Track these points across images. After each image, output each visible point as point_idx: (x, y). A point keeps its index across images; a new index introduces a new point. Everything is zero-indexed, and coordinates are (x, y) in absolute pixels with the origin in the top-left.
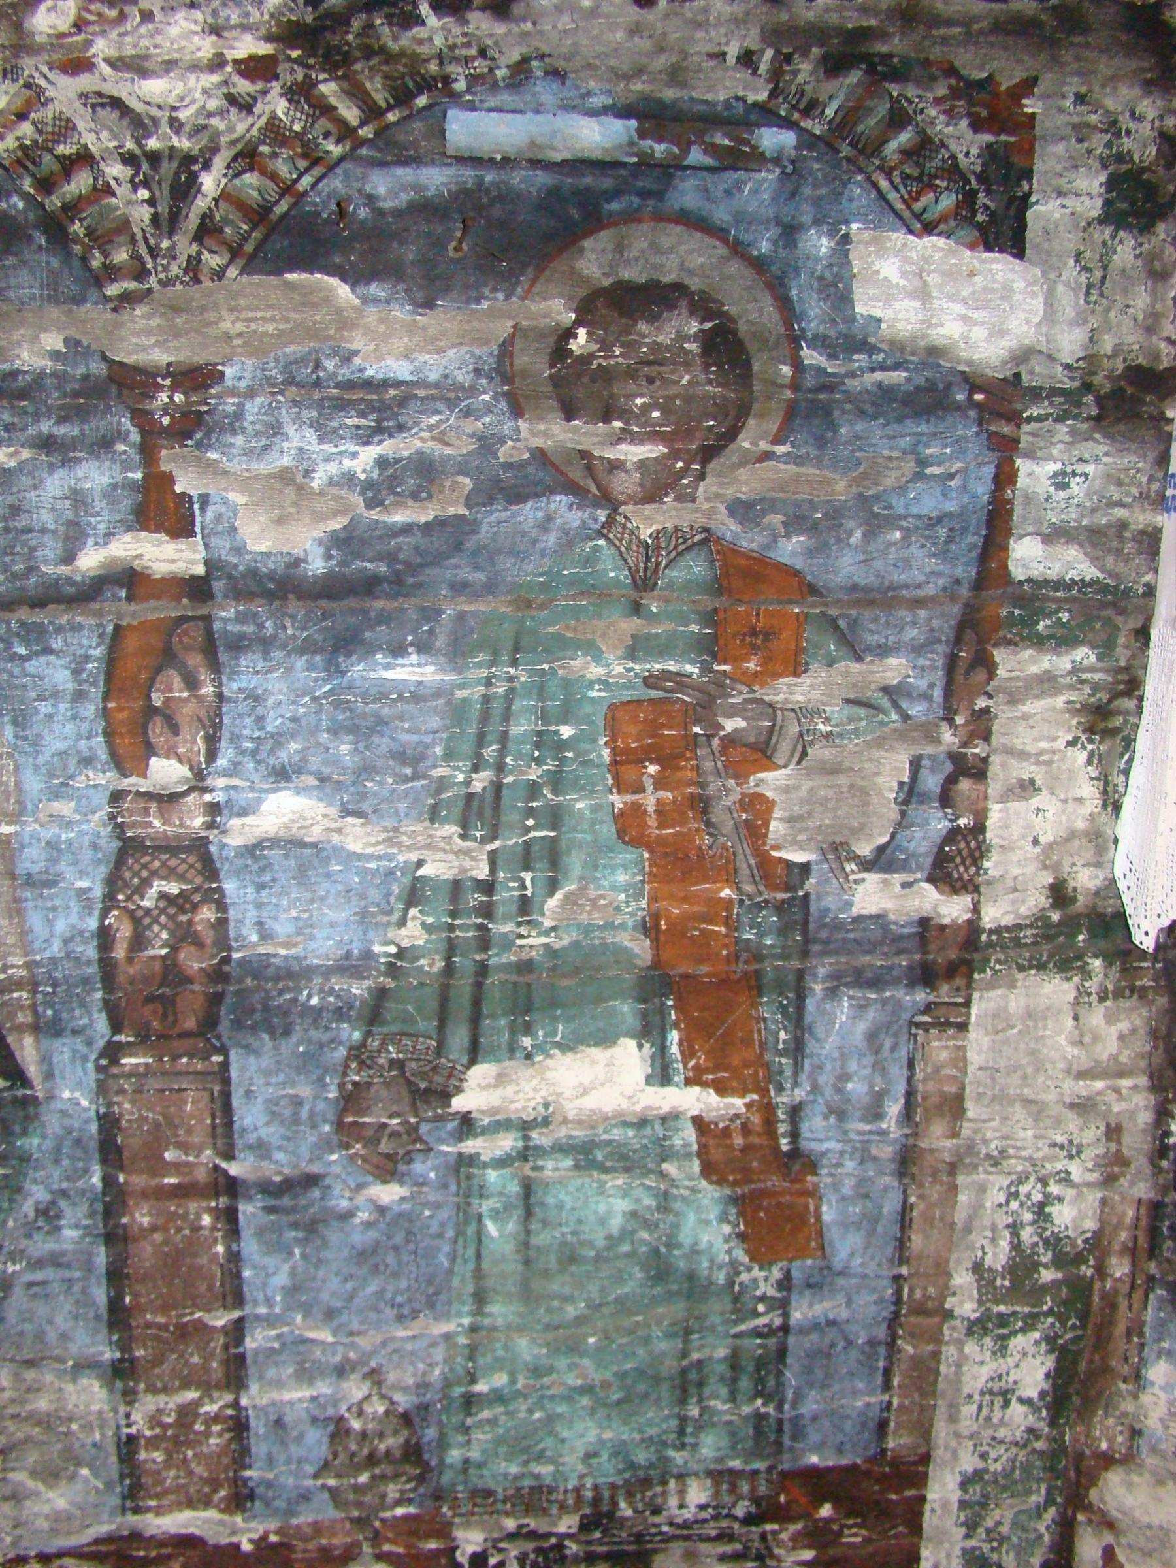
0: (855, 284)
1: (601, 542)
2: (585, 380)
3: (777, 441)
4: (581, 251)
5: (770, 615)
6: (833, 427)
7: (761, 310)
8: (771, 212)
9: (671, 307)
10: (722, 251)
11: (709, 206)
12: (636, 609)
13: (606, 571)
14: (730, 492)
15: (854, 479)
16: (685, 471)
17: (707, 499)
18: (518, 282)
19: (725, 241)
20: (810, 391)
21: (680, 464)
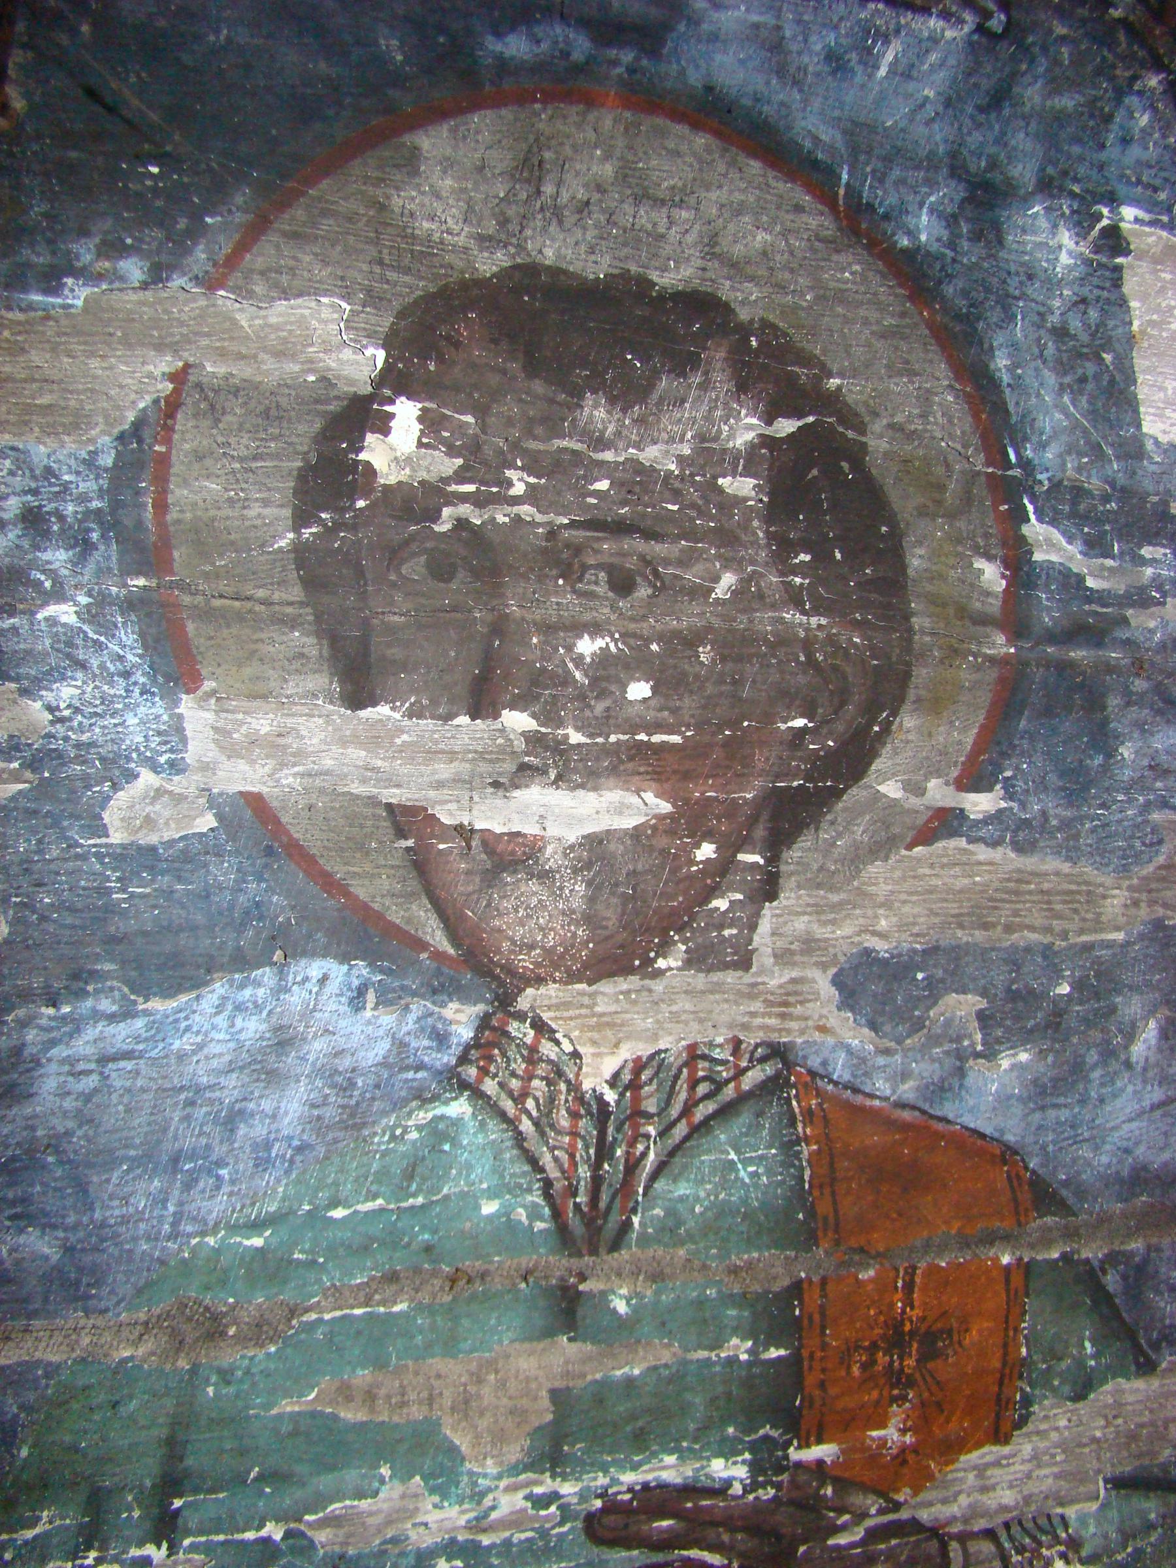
0: (1140, 362)
1: (459, 1108)
2: (415, 568)
3: (973, 778)
4: (411, 162)
5: (940, 1280)
6: (1103, 740)
7: (925, 398)
8: (936, 137)
9: (684, 363)
10: (817, 221)
11: (782, 94)
12: (567, 1309)
13: (470, 1199)
14: (844, 935)
15: (1145, 885)
16: (723, 866)
17: (783, 957)
18: (196, 231)
19: (827, 198)
20: (1051, 637)
21: (706, 851)
